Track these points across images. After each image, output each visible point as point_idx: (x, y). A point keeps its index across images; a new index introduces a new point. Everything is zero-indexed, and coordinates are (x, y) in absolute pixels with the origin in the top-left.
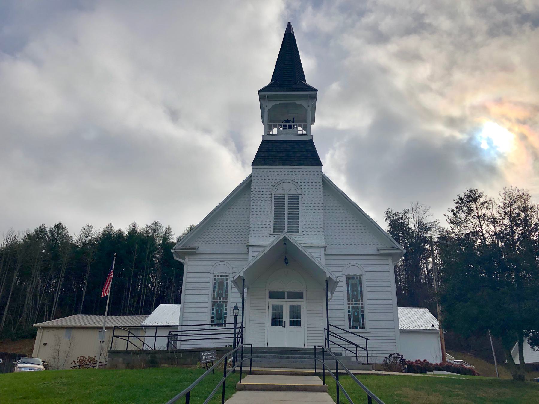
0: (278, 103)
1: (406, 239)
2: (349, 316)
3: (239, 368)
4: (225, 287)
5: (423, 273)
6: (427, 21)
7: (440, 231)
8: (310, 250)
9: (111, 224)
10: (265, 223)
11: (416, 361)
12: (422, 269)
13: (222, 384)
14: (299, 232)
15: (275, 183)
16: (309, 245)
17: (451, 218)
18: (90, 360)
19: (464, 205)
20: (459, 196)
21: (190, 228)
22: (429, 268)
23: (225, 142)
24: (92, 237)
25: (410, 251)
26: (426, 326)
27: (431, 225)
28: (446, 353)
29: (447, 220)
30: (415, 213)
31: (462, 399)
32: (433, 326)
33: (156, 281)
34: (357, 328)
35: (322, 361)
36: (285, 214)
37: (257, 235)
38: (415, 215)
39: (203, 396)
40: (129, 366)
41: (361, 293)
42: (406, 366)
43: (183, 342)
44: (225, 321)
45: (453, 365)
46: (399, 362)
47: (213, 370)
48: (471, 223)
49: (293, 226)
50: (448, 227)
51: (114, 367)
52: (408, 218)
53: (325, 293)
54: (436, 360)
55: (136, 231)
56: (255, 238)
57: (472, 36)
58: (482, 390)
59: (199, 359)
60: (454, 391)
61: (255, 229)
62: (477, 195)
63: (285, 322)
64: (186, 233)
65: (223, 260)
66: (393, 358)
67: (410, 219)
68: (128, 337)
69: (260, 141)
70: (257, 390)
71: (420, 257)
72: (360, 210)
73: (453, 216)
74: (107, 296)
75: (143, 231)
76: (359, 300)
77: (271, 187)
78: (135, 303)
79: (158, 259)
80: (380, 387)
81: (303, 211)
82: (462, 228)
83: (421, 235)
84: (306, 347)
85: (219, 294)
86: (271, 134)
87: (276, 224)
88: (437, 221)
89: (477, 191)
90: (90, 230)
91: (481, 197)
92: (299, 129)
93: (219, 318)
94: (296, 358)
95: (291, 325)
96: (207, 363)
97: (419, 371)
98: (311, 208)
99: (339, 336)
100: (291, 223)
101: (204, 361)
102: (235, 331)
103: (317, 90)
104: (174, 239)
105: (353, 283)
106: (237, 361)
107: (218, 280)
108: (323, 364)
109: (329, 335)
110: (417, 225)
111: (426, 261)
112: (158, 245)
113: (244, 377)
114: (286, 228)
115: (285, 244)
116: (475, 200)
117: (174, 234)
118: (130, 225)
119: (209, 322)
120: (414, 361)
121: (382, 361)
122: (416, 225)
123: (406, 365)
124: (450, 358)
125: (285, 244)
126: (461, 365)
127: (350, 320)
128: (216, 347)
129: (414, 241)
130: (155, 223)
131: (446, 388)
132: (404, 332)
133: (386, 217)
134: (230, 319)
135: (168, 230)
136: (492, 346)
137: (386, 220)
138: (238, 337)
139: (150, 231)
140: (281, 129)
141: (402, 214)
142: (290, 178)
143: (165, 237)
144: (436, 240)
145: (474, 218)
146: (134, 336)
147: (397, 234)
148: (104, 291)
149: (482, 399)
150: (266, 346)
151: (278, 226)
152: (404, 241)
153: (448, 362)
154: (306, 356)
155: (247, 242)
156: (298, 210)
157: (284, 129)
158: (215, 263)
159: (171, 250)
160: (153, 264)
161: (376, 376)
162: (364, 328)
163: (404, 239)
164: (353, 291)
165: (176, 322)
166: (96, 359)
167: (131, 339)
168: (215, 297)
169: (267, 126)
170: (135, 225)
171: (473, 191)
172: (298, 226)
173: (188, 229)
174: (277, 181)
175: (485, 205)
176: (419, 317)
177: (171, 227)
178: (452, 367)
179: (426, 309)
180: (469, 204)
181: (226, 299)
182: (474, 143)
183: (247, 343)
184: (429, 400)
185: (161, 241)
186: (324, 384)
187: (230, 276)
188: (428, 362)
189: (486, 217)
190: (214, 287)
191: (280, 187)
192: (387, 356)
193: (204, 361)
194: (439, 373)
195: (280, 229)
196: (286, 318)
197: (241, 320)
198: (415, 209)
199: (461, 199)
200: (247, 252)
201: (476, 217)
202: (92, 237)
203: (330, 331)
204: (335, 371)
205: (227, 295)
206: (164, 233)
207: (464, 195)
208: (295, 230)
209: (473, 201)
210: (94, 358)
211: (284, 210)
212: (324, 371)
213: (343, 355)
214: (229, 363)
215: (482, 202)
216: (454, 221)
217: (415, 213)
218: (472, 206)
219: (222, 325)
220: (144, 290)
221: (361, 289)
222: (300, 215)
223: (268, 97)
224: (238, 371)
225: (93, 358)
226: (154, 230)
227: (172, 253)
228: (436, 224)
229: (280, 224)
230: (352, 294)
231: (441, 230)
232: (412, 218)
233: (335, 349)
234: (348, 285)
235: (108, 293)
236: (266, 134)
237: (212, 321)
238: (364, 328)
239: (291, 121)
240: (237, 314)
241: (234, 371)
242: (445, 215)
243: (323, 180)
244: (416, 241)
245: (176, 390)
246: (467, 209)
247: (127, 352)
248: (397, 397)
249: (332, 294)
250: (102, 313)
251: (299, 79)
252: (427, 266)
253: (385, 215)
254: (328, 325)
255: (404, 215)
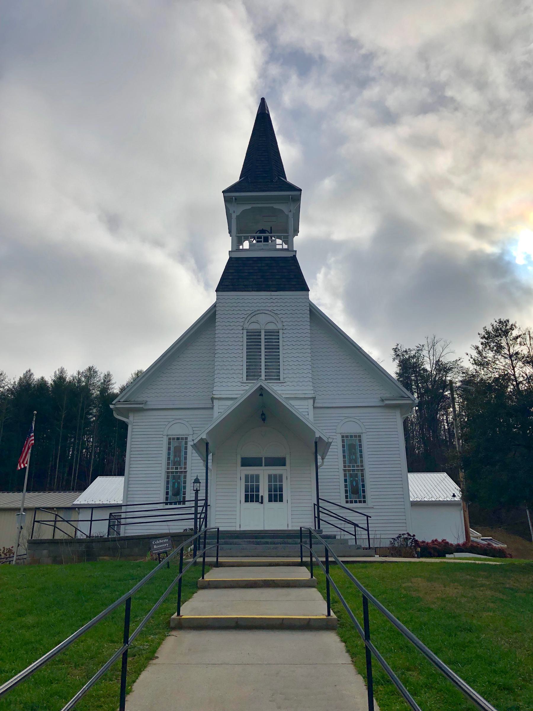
0: (248, 207)
1: (420, 383)
2: (346, 486)
3: (201, 560)
4: (183, 454)
5: (443, 427)
6: (449, 93)
7: (463, 373)
8: (293, 402)
9: (30, 371)
10: (235, 368)
11: (433, 542)
12: (441, 422)
13: (177, 581)
14: (279, 379)
15: (248, 315)
16: (293, 396)
17: (475, 358)
18: (5, 552)
19: (491, 341)
20: (484, 328)
21: (137, 374)
22: (449, 420)
23: (181, 258)
24: (5, 388)
25: (426, 399)
26: (446, 496)
27: (451, 364)
28: (470, 529)
29: (469, 360)
30: (432, 350)
31: (486, 590)
32: (454, 496)
33: (92, 446)
34: (356, 502)
35: (309, 548)
36: (261, 355)
37: (224, 384)
38: (431, 352)
39: (153, 597)
40: (56, 560)
41: (361, 456)
42: (419, 549)
43: (128, 527)
44: (184, 498)
45: (479, 544)
46: (411, 544)
47: (168, 562)
48: (501, 364)
49: (273, 370)
50: (471, 368)
51: (36, 562)
52: (422, 356)
53: (313, 457)
54: (458, 539)
55: (64, 379)
56: (223, 388)
57: (506, 112)
58: (513, 578)
59: (150, 549)
60: (477, 581)
61: (222, 376)
62: (508, 327)
63: (262, 497)
64: (132, 381)
65: (180, 417)
66: (402, 540)
67: (425, 358)
68: (55, 521)
69: (228, 258)
70: (225, 587)
71: (438, 407)
72: (359, 350)
73: (477, 355)
74: (25, 468)
75: (73, 379)
76: (358, 466)
77: (243, 320)
78: (66, 475)
79: (95, 416)
80: (383, 578)
81: (285, 352)
82: (490, 371)
83: (439, 378)
84: (290, 528)
85: (175, 463)
86: (241, 249)
87: (250, 369)
88: (459, 360)
89: (508, 322)
90: (2, 378)
91: (513, 329)
92: (279, 241)
93: (177, 493)
94: (277, 544)
95: (270, 500)
96: (159, 554)
97: (436, 554)
98: (295, 347)
99: (332, 513)
100: (270, 367)
101: (156, 552)
102: (196, 510)
103: (300, 190)
104: (116, 389)
105: (350, 444)
106: (199, 550)
107: (174, 444)
108: (310, 551)
109: (320, 513)
110: (434, 366)
111: (447, 412)
112: (95, 398)
113: (208, 571)
114: (263, 374)
115: (261, 395)
116: (506, 333)
117: (116, 382)
118: (56, 372)
119: (162, 499)
120: (430, 541)
121: (389, 543)
122: (433, 366)
123: (418, 548)
124: (476, 536)
125: (261, 395)
126: (489, 544)
127: (346, 491)
128: (171, 531)
129: (430, 387)
130: (90, 369)
131: (468, 577)
132: (417, 504)
133: (393, 356)
134: (190, 495)
135: (108, 377)
136: (529, 519)
137: (394, 359)
138: (200, 518)
139: (83, 379)
140: (254, 242)
141: (415, 351)
142: (267, 308)
143: (103, 387)
144: (458, 384)
145: (504, 357)
146: (64, 521)
147: (409, 378)
148: (21, 461)
149: (512, 589)
150: (238, 529)
151: (253, 372)
152: (418, 386)
153: (473, 541)
154: (290, 541)
155: (211, 393)
156: (278, 350)
157: (257, 242)
158: (169, 422)
159: (110, 405)
160: (88, 423)
161: (379, 564)
162: (364, 502)
163: (418, 385)
164: (350, 454)
165: (118, 500)
166: (14, 550)
167: (58, 524)
168: (170, 467)
169: (235, 238)
170: (62, 371)
171: (504, 322)
172: (279, 371)
173: (134, 376)
174: (249, 312)
175: (519, 340)
176: (436, 484)
177: (111, 373)
178: (477, 547)
179: (445, 474)
180: (499, 339)
181: (185, 468)
182: (507, 258)
183: (212, 526)
184: (445, 594)
185: (99, 393)
186: (312, 577)
187: (190, 438)
188: (447, 543)
189: (519, 356)
190: (169, 454)
191: (253, 319)
192: (395, 536)
193: (156, 552)
194: (461, 556)
195: (254, 376)
196: (264, 492)
197: (204, 495)
198: (431, 344)
199: (488, 333)
200: (210, 406)
201: (507, 356)
202: (5, 388)
203: (321, 507)
204: (324, 559)
205: (185, 463)
206: (102, 381)
207: (492, 327)
208: (275, 376)
209: (503, 335)
210: (11, 548)
211: (259, 350)
212: (311, 559)
213: (338, 537)
214: (189, 553)
215: (514, 336)
216: (478, 361)
217: (432, 350)
218: (502, 341)
219: (180, 503)
220: (77, 457)
221: (361, 451)
222: (281, 357)
223: (236, 199)
224: (200, 562)
225: (9, 548)
226: (89, 377)
227: (111, 410)
228: (458, 363)
229: (255, 369)
230: (350, 457)
231: (465, 371)
232: (428, 356)
233: (327, 530)
234: (343, 446)
235: (27, 463)
236: (235, 249)
237: (167, 499)
238: (364, 502)
239: (267, 231)
240: (198, 489)
241: (195, 563)
242: (467, 354)
243: (310, 311)
244: (433, 386)
245: (118, 591)
246: (495, 346)
247: (53, 542)
248: (405, 592)
249: (323, 459)
250: (20, 490)
251: (277, 175)
252: (447, 418)
253: (393, 353)
254: (318, 499)
255: (418, 352)
